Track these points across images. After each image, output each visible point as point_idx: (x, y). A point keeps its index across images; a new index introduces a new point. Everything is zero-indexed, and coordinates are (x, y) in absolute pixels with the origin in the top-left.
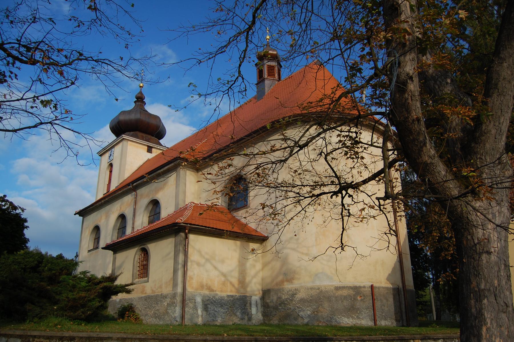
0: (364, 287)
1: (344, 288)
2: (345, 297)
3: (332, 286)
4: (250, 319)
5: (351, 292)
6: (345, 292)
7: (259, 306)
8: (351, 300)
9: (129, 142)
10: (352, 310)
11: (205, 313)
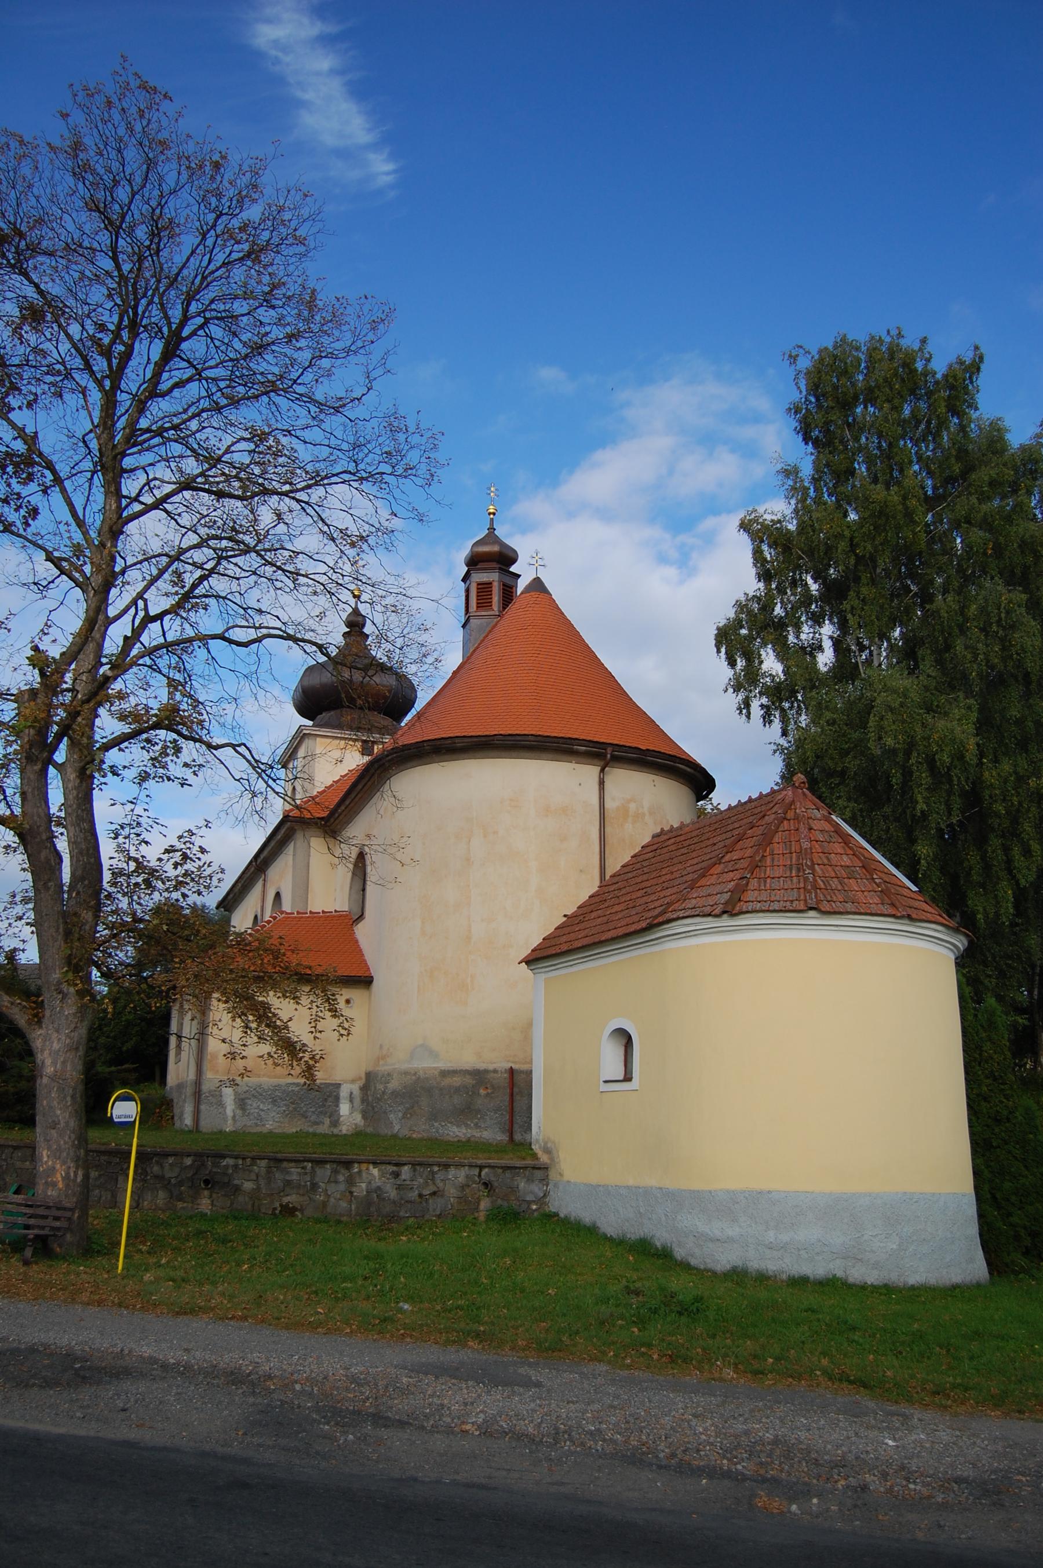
0: (495, 1071)
1: (454, 1072)
2: (457, 1090)
3: (435, 1068)
4: (335, 1123)
5: (469, 1080)
6: (457, 1081)
7: (357, 1101)
8: (467, 1093)
9: (318, 739)
10: (466, 1112)
11: (239, 1112)
